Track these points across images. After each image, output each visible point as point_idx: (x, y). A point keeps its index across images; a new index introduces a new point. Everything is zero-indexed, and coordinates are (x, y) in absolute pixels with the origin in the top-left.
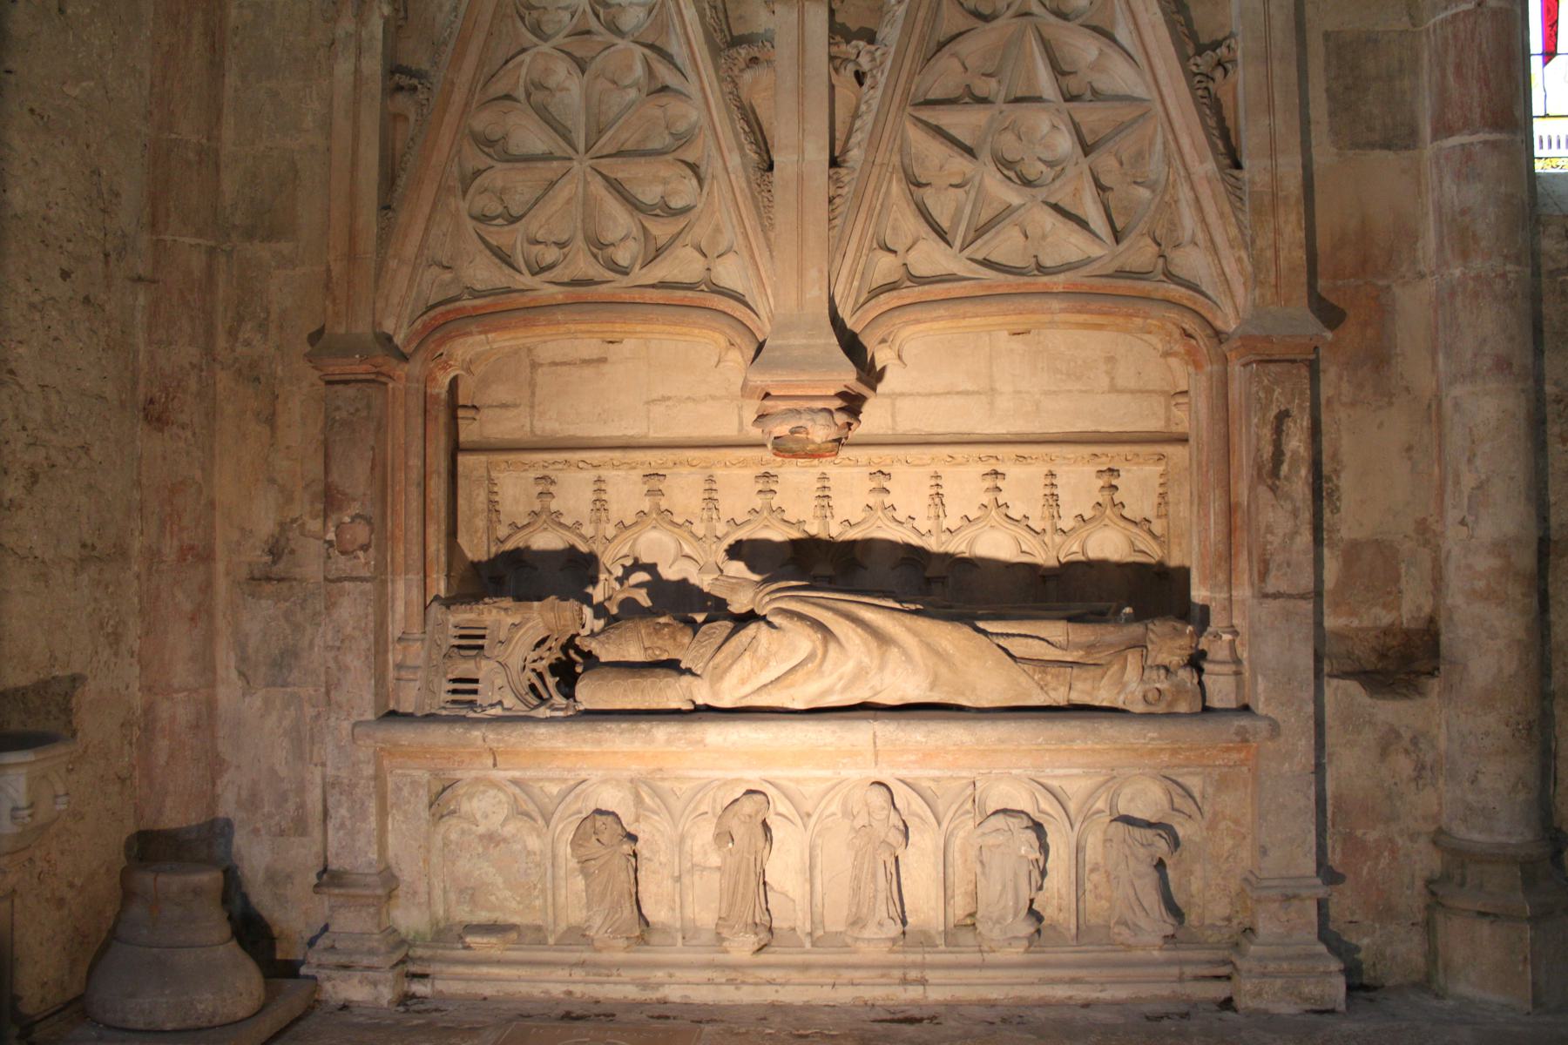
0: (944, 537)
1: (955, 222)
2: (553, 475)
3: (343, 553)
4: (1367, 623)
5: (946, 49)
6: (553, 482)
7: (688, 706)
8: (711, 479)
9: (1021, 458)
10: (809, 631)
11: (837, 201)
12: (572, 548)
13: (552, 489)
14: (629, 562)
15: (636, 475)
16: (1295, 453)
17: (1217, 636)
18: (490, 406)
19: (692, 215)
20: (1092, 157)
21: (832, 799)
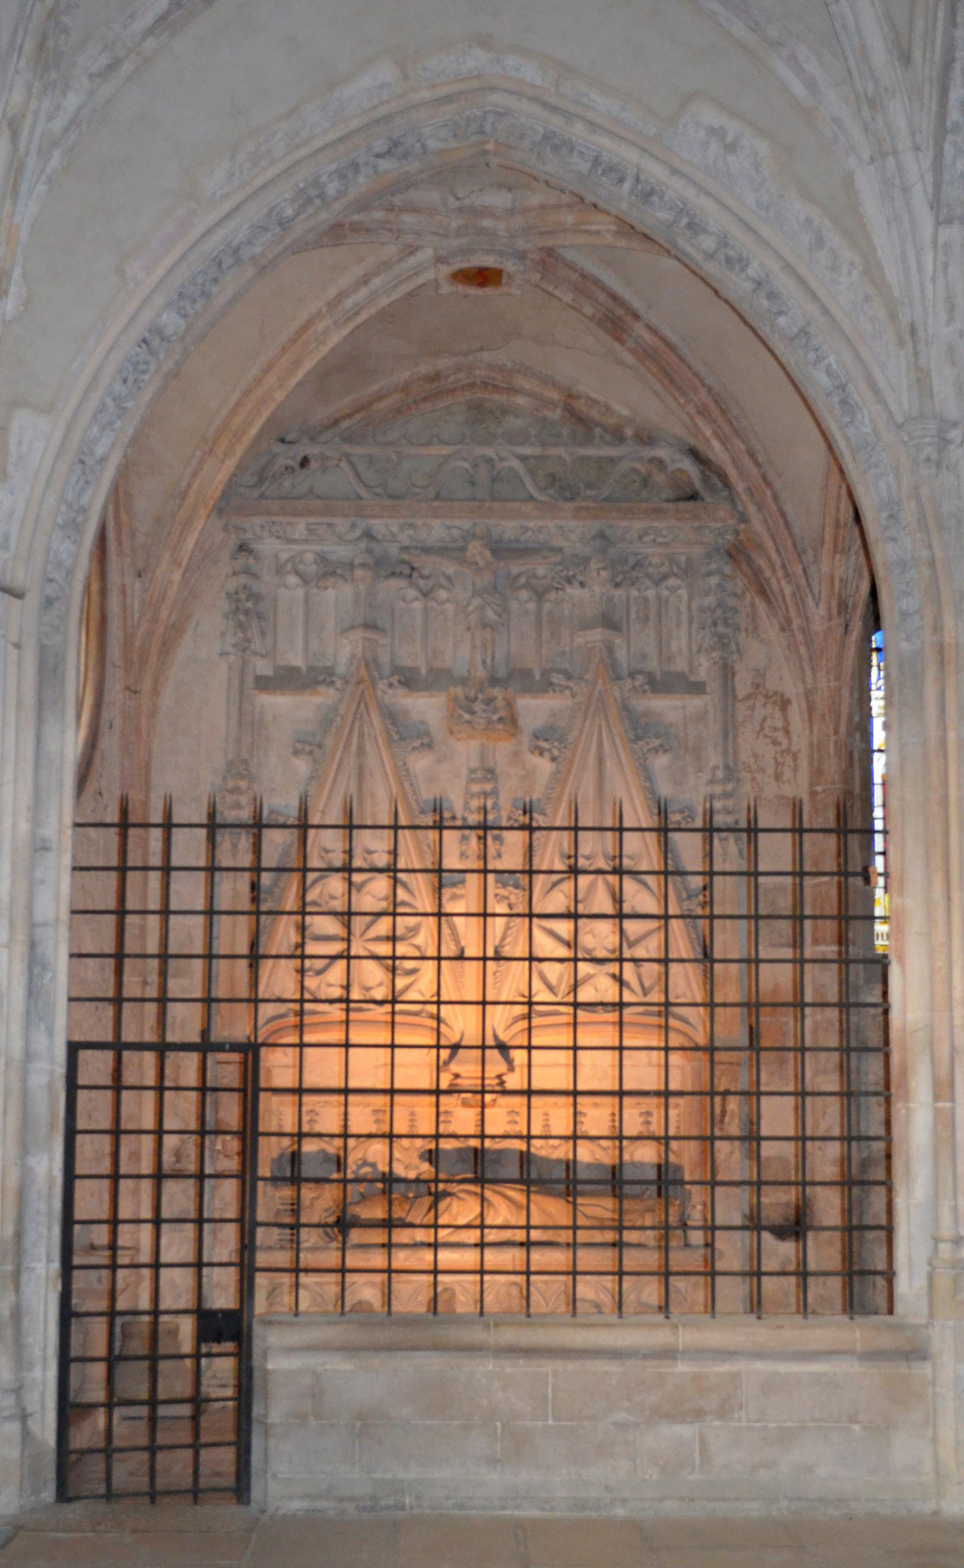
0: (550, 1150)
1: (559, 984)
2: (317, 1109)
3: (227, 1156)
4: (774, 1201)
5: (557, 888)
6: (317, 1114)
7: (411, 1242)
8: (413, 1114)
9: (596, 1105)
10: (882, 1039)
11: (498, 974)
12: (323, 1151)
13: (317, 1118)
14: (360, 1162)
15: (368, 1111)
16: (732, 1111)
17: (694, 1207)
18: (279, 1067)
19: (419, 974)
20: (632, 949)
21: (660, 890)
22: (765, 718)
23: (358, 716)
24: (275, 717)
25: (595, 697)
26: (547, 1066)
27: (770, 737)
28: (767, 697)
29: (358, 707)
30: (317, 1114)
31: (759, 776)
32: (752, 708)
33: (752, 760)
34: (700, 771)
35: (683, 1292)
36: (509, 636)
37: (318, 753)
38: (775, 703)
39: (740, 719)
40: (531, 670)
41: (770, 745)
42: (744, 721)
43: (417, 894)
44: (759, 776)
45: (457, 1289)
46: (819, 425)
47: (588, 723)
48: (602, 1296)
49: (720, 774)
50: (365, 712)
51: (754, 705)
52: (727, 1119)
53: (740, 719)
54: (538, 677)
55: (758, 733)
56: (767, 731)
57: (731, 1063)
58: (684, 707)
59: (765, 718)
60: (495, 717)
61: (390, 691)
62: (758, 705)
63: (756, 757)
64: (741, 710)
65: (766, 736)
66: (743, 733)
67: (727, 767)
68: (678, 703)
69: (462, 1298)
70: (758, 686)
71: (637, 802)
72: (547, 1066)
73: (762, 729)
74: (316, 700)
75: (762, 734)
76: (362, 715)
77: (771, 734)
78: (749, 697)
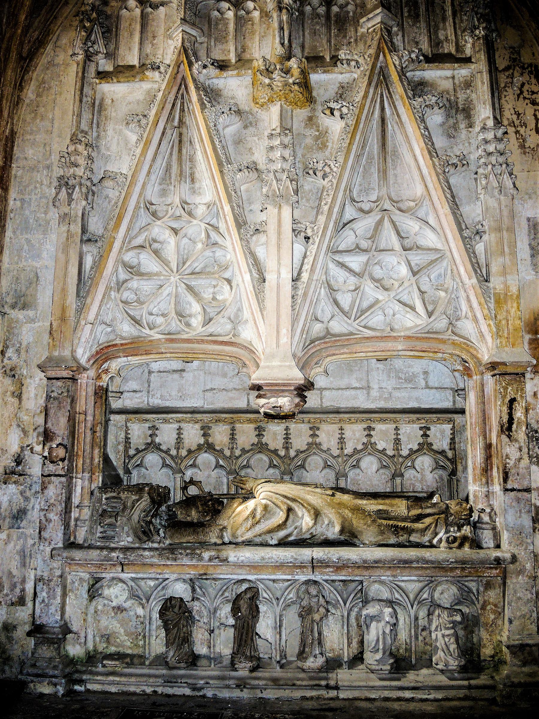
6: (157, 429)
15: (198, 426)
16: (519, 419)
22: (523, 85)
23: (180, 96)
24: (113, 101)
25: (377, 71)
26: (342, 389)
27: (529, 99)
28: (523, 68)
29: (179, 89)
30: (157, 429)
31: (522, 130)
32: (512, 77)
33: (515, 117)
34: (471, 127)
35: (475, 591)
36: (303, 31)
37: (144, 121)
38: (530, 73)
39: (502, 85)
40: (323, 57)
41: (530, 105)
42: (505, 87)
43: (226, 235)
44: (522, 130)
45: (261, 586)
46: (444, 232)
47: (372, 91)
48: (397, 596)
49: (490, 123)
50: (185, 93)
51: (513, 74)
52: (514, 426)
53: (502, 85)
54: (328, 60)
55: (519, 96)
56: (525, 94)
57: (517, 374)
58: (453, 78)
59: (523, 85)
60: (291, 81)
61: (204, 71)
62: (516, 74)
63: (518, 115)
64: (503, 79)
65: (525, 98)
66: (505, 96)
67: (495, 118)
68: (449, 73)
69: (265, 595)
70: (514, 60)
71: (418, 152)
72: (342, 389)
73: (522, 92)
74: (146, 86)
75: (522, 96)
76: (183, 95)
77: (529, 96)
78: (507, 69)
